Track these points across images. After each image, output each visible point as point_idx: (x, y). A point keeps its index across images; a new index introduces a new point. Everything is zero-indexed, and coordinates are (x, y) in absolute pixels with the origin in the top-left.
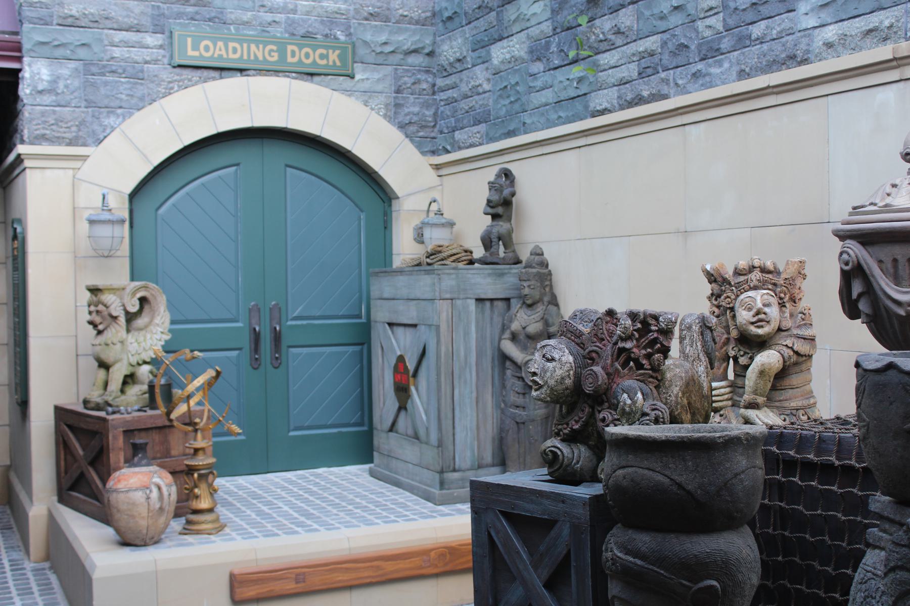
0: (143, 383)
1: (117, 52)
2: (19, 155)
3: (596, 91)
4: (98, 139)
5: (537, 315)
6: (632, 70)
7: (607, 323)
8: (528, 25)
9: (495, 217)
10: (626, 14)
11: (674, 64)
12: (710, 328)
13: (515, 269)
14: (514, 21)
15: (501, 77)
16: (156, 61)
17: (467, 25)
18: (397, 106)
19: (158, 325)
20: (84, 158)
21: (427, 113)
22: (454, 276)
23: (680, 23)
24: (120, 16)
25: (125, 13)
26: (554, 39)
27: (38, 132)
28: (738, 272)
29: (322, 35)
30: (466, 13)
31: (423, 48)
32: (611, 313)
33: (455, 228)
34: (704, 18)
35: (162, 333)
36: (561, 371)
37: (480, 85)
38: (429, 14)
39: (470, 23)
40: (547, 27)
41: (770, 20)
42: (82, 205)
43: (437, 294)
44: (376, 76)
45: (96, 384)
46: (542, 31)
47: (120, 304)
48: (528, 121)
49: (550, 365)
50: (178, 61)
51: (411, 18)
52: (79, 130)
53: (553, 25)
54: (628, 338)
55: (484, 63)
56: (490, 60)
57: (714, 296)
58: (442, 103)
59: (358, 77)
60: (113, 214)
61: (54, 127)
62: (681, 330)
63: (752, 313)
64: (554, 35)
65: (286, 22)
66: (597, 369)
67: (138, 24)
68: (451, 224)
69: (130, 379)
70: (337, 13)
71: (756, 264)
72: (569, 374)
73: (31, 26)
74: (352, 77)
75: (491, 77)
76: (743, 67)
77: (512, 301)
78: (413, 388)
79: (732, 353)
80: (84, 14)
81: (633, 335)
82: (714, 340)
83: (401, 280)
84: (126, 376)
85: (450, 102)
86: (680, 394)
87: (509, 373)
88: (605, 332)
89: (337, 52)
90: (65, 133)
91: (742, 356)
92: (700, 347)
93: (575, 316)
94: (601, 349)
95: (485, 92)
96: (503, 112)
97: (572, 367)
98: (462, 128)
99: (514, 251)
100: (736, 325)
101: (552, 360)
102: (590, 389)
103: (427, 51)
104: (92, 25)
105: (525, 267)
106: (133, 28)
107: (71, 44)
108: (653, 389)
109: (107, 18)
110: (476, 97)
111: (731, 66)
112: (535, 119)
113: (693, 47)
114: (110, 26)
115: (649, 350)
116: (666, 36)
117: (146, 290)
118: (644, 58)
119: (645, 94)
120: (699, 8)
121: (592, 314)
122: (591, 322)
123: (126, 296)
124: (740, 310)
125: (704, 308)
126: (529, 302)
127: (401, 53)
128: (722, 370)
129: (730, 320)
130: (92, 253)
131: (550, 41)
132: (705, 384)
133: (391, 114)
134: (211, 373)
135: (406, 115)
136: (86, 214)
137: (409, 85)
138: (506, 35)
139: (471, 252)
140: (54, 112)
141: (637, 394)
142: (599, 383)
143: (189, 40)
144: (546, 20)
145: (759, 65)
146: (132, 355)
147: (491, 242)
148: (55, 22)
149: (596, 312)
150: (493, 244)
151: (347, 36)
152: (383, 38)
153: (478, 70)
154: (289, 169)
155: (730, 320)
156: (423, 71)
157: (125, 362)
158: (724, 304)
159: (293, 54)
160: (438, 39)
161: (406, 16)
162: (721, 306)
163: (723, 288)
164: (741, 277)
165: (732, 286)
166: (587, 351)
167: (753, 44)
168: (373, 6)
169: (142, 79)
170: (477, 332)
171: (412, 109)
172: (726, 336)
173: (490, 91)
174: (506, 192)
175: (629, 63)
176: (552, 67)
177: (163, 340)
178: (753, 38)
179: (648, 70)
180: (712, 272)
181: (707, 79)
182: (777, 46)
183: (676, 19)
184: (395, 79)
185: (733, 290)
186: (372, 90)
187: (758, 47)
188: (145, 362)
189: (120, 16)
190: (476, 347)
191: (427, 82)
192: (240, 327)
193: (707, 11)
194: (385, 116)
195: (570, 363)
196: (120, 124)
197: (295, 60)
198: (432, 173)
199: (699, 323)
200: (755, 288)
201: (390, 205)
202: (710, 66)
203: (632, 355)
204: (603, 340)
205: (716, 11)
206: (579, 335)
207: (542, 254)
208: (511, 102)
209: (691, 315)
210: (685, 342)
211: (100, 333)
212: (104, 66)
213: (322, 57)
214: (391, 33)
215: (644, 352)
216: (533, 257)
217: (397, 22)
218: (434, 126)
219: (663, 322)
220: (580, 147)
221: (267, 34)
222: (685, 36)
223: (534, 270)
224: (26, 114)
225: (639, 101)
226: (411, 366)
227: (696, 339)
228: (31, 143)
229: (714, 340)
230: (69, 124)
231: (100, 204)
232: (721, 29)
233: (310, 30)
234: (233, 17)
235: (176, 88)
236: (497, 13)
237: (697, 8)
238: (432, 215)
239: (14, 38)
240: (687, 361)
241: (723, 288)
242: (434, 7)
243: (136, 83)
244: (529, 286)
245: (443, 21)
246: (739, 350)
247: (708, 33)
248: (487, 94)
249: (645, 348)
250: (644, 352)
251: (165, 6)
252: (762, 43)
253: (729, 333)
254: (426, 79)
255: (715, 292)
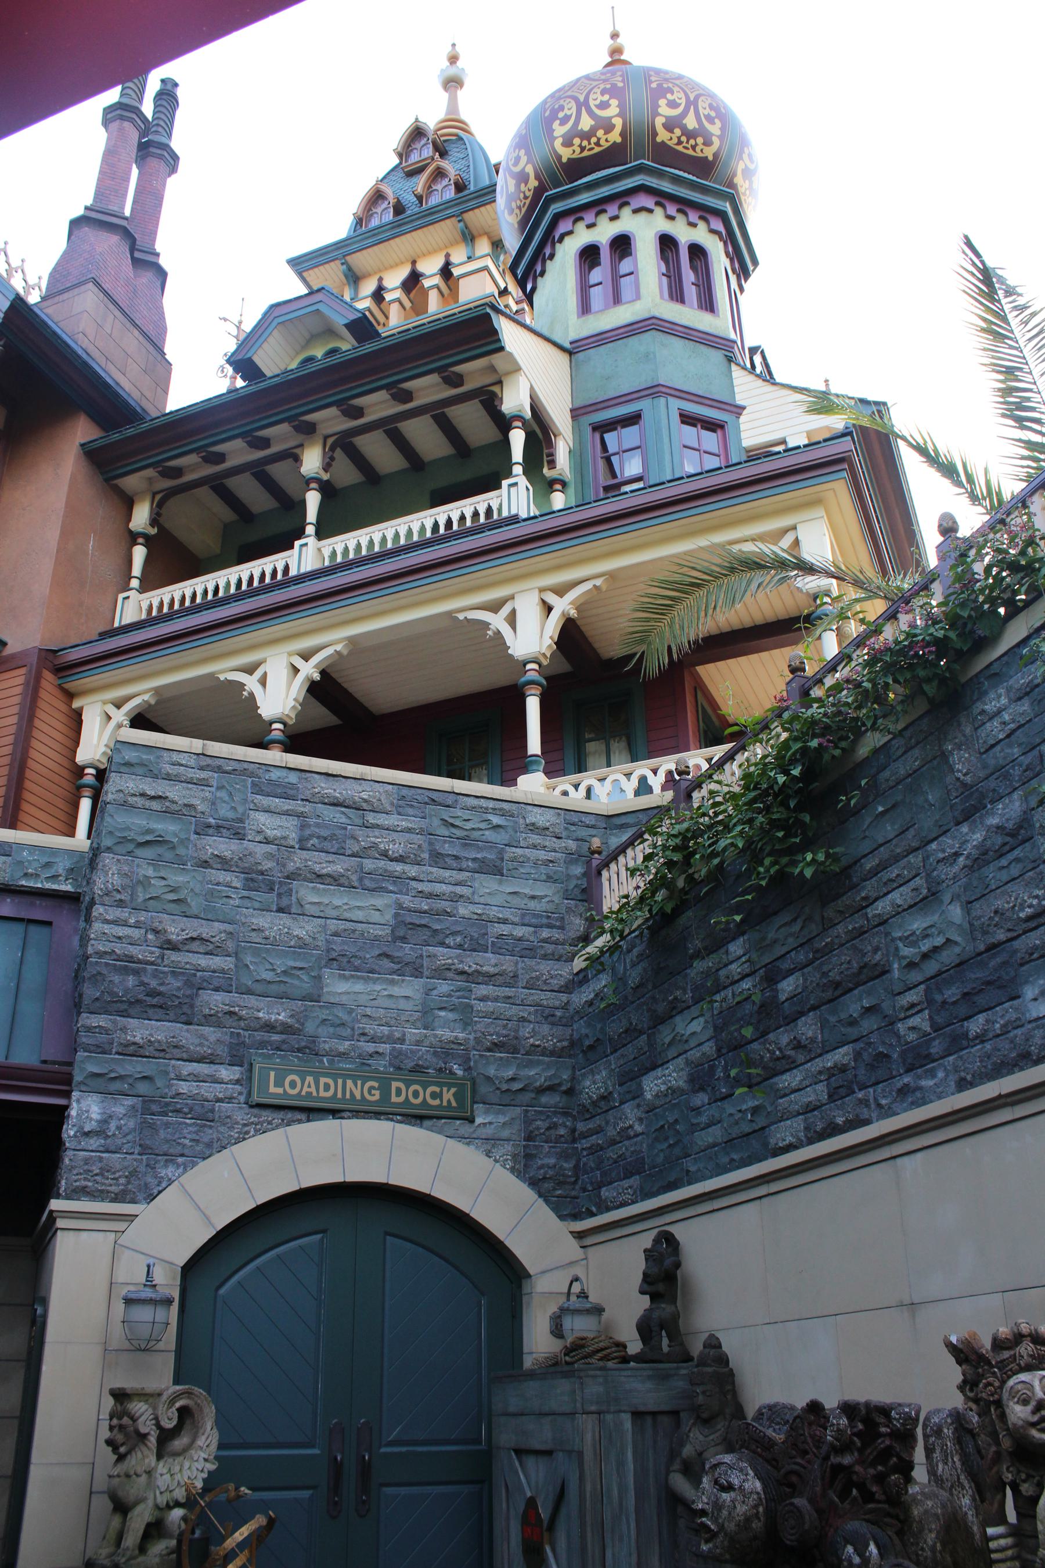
0: (171, 1537)
1: (184, 1087)
2: (51, 1212)
3: (776, 1123)
4: (151, 1195)
5: (718, 1434)
6: (819, 1092)
7: (810, 1424)
8: (687, 1047)
9: (655, 1297)
10: (806, 1023)
11: (873, 1080)
12: (970, 1432)
13: (685, 1368)
14: (670, 1044)
15: (655, 1115)
16: (230, 1099)
17: (612, 1053)
18: (529, 1157)
19: (201, 1448)
20: (131, 1218)
21: (566, 1165)
22: (601, 1380)
23: (875, 1027)
24: (192, 1044)
25: (197, 1041)
26: (720, 1062)
27: (78, 1184)
28: (998, 1344)
29: (435, 1069)
30: (610, 1040)
31: (560, 1085)
32: (815, 1407)
33: (605, 1315)
34: (905, 1018)
35: (206, 1460)
36: (745, 1507)
37: (631, 1127)
38: (565, 1044)
39: (615, 1051)
40: (709, 1048)
41: (990, 1012)
42: (121, 1280)
43: (579, 1405)
44: (502, 1119)
45: (107, 1537)
46: (704, 1054)
47: (152, 1417)
48: (693, 1169)
49: (726, 1496)
50: (256, 1098)
51: (545, 1047)
52: (129, 1183)
53: (716, 1045)
54: (844, 1447)
55: (634, 1098)
56: (642, 1094)
57: (967, 1385)
58: (585, 1153)
59: (479, 1120)
60: (157, 1291)
61: (98, 1178)
62: (926, 1437)
63: (1029, 1408)
64: (719, 1057)
65: (390, 1054)
66: (800, 1502)
67: (211, 1054)
68: (598, 1310)
69: (155, 1529)
70: (453, 1043)
71: (1025, 1329)
72: (758, 1512)
73: (86, 1054)
74: (472, 1121)
75: (643, 1115)
76: (963, 1074)
77: (682, 1415)
78: (548, 1549)
79: (1008, 1477)
80: (150, 1041)
81: (853, 1443)
82: (979, 1452)
83: (531, 1388)
84: (149, 1525)
85: (594, 1150)
86: (939, 1546)
87: (682, 1523)
88: (809, 1440)
89: (453, 1090)
90: (111, 1185)
91: (1024, 1481)
92: (958, 1464)
93: (759, 1415)
94: (805, 1468)
95: (637, 1135)
96: (660, 1159)
97: (760, 1499)
98: (610, 1183)
99: (682, 1344)
100: (1008, 1429)
101: (729, 1488)
102: (793, 1538)
103: (564, 1088)
104: (157, 1054)
105: (697, 1366)
106: (205, 1058)
107: (130, 1076)
108: (894, 1537)
109: (176, 1047)
110: (626, 1143)
111: (947, 1076)
112: (701, 1166)
113: (895, 1056)
114: (178, 1056)
115: (880, 1468)
116: (860, 1045)
117: (189, 1398)
118: (834, 1075)
119: (840, 1120)
120: (898, 1006)
121: (786, 1410)
122: (785, 1424)
123: (161, 1406)
124: (1011, 1403)
125: (957, 1401)
126: (705, 1415)
127: (532, 1091)
128: (996, 1505)
129: (997, 1422)
130: (127, 1345)
131: (714, 1065)
132: (975, 1528)
133: (520, 1167)
134: (259, 1521)
135: (540, 1168)
136: (124, 1292)
137: (542, 1131)
138: (660, 1062)
139: (625, 1347)
140: (101, 1159)
141: (868, 1545)
142: (807, 1527)
143: (272, 1074)
144: (708, 1040)
145: (983, 1070)
146: (161, 1493)
147: (651, 1331)
148: (114, 1051)
149: (792, 1408)
150: (654, 1334)
151: (465, 1070)
152: (510, 1073)
153: (627, 1108)
154: (388, 1237)
155: (997, 1422)
156: (559, 1113)
157: (150, 1503)
158: (984, 1395)
159: (399, 1092)
160: (578, 1073)
161: (539, 1046)
162: (981, 1399)
163: (980, 1370)
164: (1005, 1352)
165: (993, 1367)
166: (783, 1471)
167: (971, 1044)
168: (498, 1034)
169: (212, 1121)
170: (635, 1461)
171: (546, 1161)
172: (993, 1449)
173: (643, 1133)
174: (668, 1262)
175: (816, 1083)
176: (718, 1097)
177: (206, 1470)
178: (971, 1036)
179: (841, 1090)
180: (960, 1346)
181: (918, 1094)
182: (1004, 1044)
183: (869, 1024)
184: (525, 1122)
185: (995, 1373)
186: (496, 1136)
187: (979, 1047)
188: (178, 1504)
189: (192, 1044)
190: (635, 1482)
191: (566, 1126)
192: (315, 1455)
193: (908, 1009)
194: (512, 1170)
195: (758, 1493)
196: (179, 1176)
197: (401, 1099)
198: (573, 1243)
199: (952, 1423)
200: (1029, 1368)
201: (520, 1287)
202: (920, 1078)
203: (855, 1477)
204: (805, 1452)
205: (919, 1008)
206: (768, 1444)
207: (720, 1346)
208: (670, 1146)
209: (938, 1411)
210: (935, 1455)
211: (121, 1458)
212: (167, 1104)
213: (434, 1095)
214: (518, 1067)
215: (872, 1471)
216: (707, 1350)
217: (527, 1054)
218: (575, 1183)
219: (898, 1420)
220: (760, 1198)
221: (367, 1068)
222: (884, 1043)
223: (709, 1370)
224: (67, 1161)
225: (833, 1130)
226: (544, 1513)
227: (951, 1452)
228: (68, 1198)
229: (979, 1452)
230: (117, 1175)
231: (143, 1279)
232: (928, 1029)
233: (421, 1063)
234: (327, 1047)
235: (252, 1133)
236: (648, 1037)
237: (894, 1007)
238: (573, 1298)
239: (64, 1069)
240: (942, 1488)
241: (980, 1370)
242: (572, 1035)
243: (205, 1126)
244: (704, 1393)
245: (583, 1051)
246: (1019, 1472)
247: (912, 1037)
248: (640, 1137)
249: (873, 1464)
250: (872, 1471)
251: (247, 1034)
252: (983, 1042)
253: (997, 1443)
254: (564, 1123)
255: (969, 1377)
